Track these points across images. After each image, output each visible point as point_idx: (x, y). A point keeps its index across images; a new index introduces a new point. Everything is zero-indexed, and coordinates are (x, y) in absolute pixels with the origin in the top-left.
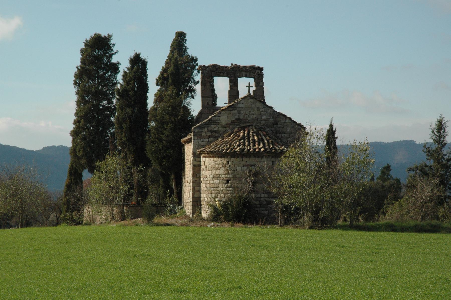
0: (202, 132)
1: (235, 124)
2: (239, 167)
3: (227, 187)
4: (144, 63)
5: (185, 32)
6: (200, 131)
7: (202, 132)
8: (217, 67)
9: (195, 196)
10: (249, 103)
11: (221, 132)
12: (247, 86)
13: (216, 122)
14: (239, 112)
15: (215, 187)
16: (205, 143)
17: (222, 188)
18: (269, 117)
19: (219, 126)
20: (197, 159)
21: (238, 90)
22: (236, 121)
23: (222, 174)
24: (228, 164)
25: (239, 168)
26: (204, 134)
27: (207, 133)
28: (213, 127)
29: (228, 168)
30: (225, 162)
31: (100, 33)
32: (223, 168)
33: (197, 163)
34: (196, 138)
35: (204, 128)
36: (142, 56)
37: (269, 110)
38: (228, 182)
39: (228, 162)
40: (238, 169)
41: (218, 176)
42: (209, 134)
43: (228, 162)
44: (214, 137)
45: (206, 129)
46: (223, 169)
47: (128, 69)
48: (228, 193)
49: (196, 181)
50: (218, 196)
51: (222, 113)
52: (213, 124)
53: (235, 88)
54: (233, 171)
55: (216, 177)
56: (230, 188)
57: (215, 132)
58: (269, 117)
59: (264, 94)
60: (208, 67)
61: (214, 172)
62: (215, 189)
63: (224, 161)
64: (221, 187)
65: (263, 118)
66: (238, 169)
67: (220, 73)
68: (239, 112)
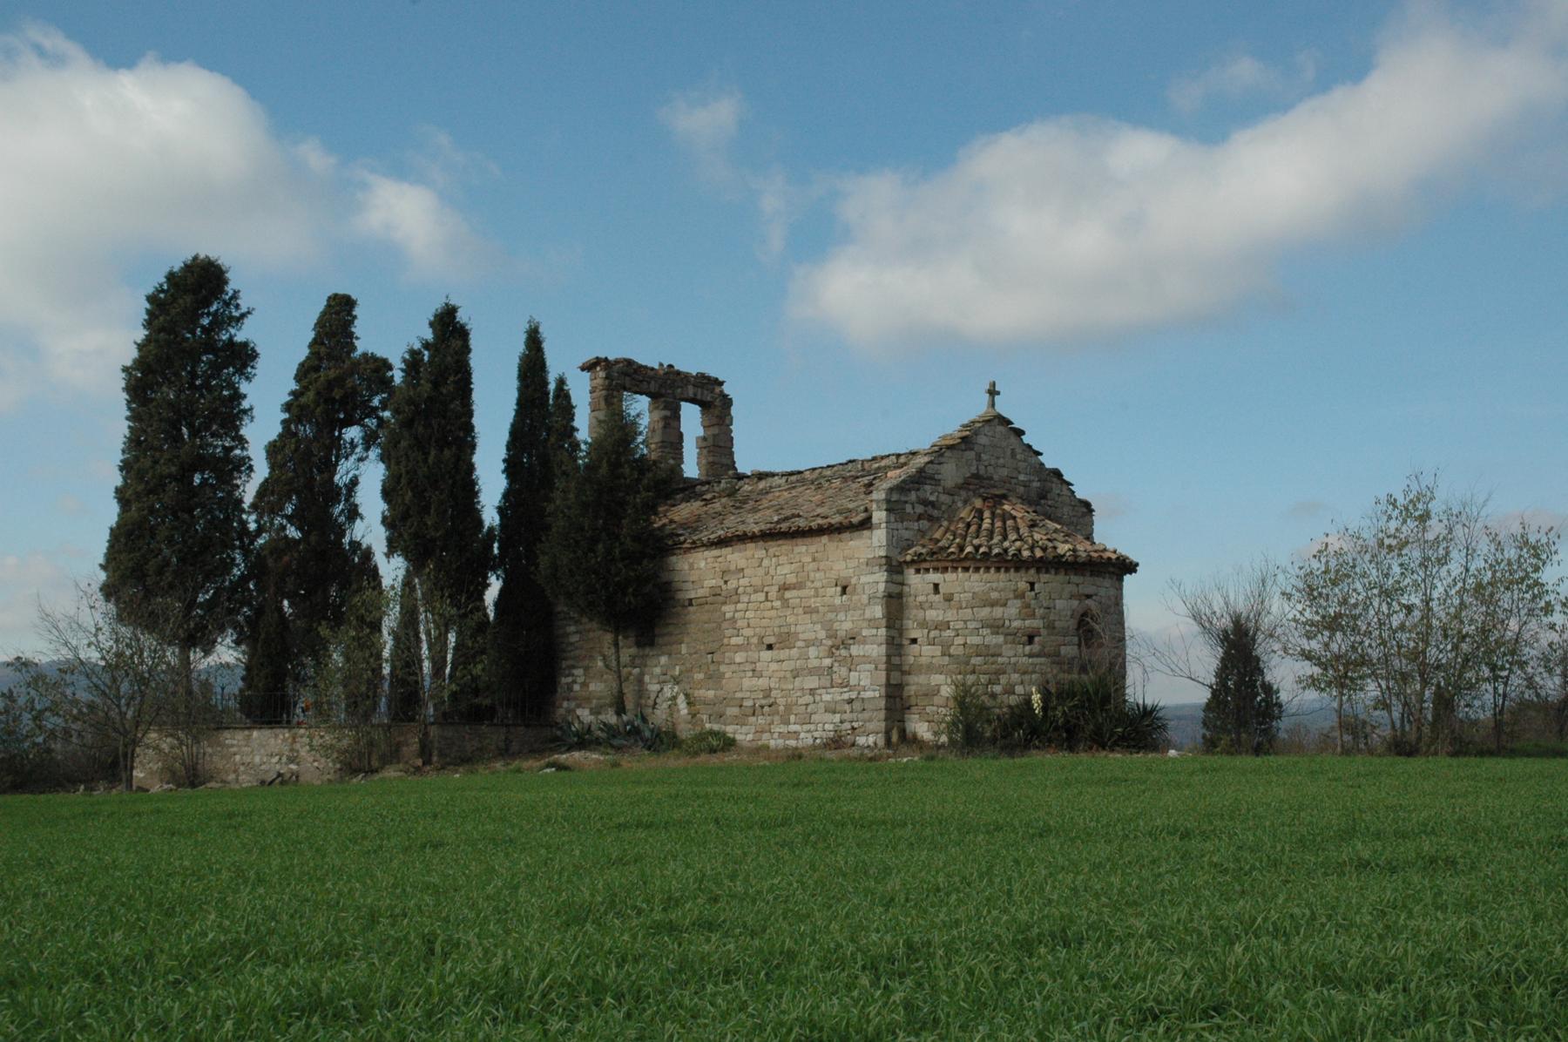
0: (906, 502)
1: (971, 487)
2: (1060, 598)
3: (1031, 656)
4: (462, 333)
5: (354, 297)
6: (903, 499)
7: (906, 502)
8: (635, 367)
9: (892, 682)
10: (997, 436)
11: (944, 508)
12: (998, 393)
13: (933, 479)
14: (979, 458)
15: (988, 655)
16: (912, 533)
17: (1015, 656)
18: (1032, 478)
19: (940, 489)
20: (897, 578)
21: (682, 430)
22: (973, 480)
23: (1013, 617)
24: (1032, 589)
25: (1062, 601)
26: (909, 508)
27: (916, 505)
28: (928, 492)
29: (1033, 602)
30: (1023, 585)
31: (213, 255)
32: (1015, 601)
33: (895, 589)
34: (893, 519)
35: (909, 490)
36: (461, 316)
37: (1033, 460)
38: (1031, 639)
39: (1032, 585)
40: (1060, 604)
41: (1001, 622)
42: (920, 509)
43: (1032, 585)
44: (931, 519)
45: (913, 496)
46: (1018, 603)
47: (427, 345)
48: (1035, 672)
49: (893, 638)
50: (999, 680)
51: (946, 454)
52: (928, 482)
53: (674, 424)
54: (1047, 611)
55: (990, 627)
56: (1038, 656)
57: (933, 504)
58: (1032, 478)
59: (732, 444)
60: (617, 362)
61: (985, 612)
62: (992, 659)
63: (1020, 581)
64: (1011, 653)
65: (1022, 477)
66: (1060, 604)
67: (641, 381)
68: (979, 458)
